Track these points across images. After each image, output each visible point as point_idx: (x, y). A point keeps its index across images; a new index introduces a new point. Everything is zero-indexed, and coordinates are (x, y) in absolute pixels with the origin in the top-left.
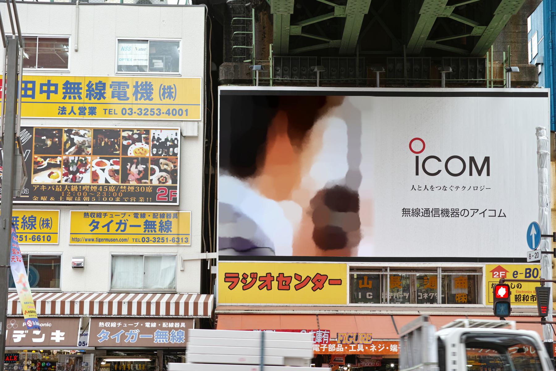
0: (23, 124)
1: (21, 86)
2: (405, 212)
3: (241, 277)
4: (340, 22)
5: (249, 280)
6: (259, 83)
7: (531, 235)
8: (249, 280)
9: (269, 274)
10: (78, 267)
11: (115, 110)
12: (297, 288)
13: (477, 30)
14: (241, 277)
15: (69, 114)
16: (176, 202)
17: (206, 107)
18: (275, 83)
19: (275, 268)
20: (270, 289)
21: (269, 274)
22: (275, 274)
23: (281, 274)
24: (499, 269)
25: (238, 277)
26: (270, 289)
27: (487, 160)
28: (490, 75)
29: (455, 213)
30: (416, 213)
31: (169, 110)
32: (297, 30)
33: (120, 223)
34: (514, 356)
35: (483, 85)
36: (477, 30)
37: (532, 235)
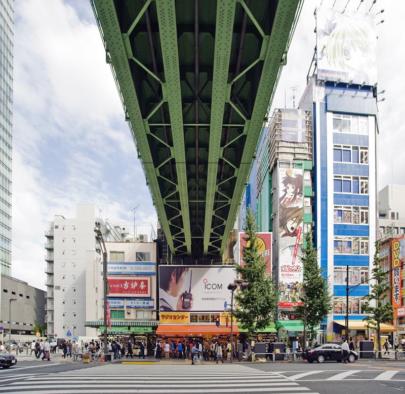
2: (203, 299)
4: (185, 247)
10: (129, 313)
11: (398, 213)
12: (178, 319)
13: (219, 249)
16: (147, 293)
17: (194, 266)
18: (173, 264)
19: (173, 314)
24: (224, 314)
27: (221, 285)
28: (223, 262)
29: (214, 299)
30: (205, 299)
32: (176, 249)
35: (222, 264)
36: (219, 249)
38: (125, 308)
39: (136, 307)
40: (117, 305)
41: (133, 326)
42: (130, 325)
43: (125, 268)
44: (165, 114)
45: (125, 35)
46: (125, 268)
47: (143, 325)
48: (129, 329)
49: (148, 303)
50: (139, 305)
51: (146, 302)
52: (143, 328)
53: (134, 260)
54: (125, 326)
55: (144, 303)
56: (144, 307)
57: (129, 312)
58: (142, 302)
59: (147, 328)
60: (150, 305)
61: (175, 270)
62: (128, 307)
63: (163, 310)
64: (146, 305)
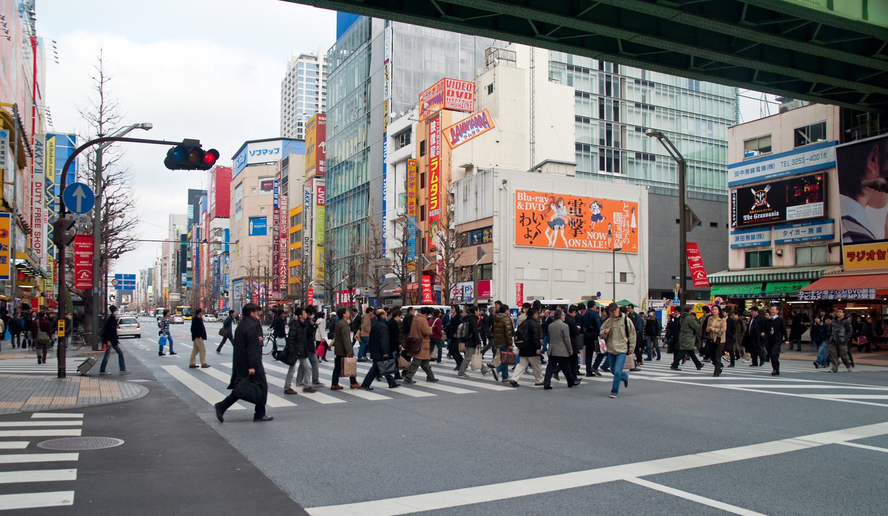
0: (674, 180)
1: (748, 159)
3: (856, 254)
5: (861, 255)
6: (849, 110)
7: (74, 195)
8: (861, 255)
9: (872, 251)
10: (780, 255)
14: (856, 254)
15: (41, 167)
20: (873, 259)
21: (872, 251)
22: (876, 251)
23: (879, 251)
25: (854, 254)
26: (873, 259)
31: (42, 145)
33: (797, 231)
34: (7, 330)
37: (76, 196)
38: (773, 246)
39: (793, 242)
40: (756, 241)
41: (773, 282)
42: (767, 279)
43: (771, 166)
44: (538, 24)
45: (443, 17)
46: (771, 166)
47: (792, 278)
48: (764, 287)
49: (819, 230)
50: (801, 235)
51: (815, 227)
52: (792, 285)
53: (790, 144)
54: (757, 282)
55: (811, 231)
56: (811, 240)
57: (779, 252)
58: (806, 228)
59: (802, 284)
60: (824, 233)
61: (877, 146)
62: (779, 243)
63: (850, 241)
64: (815, 234)
